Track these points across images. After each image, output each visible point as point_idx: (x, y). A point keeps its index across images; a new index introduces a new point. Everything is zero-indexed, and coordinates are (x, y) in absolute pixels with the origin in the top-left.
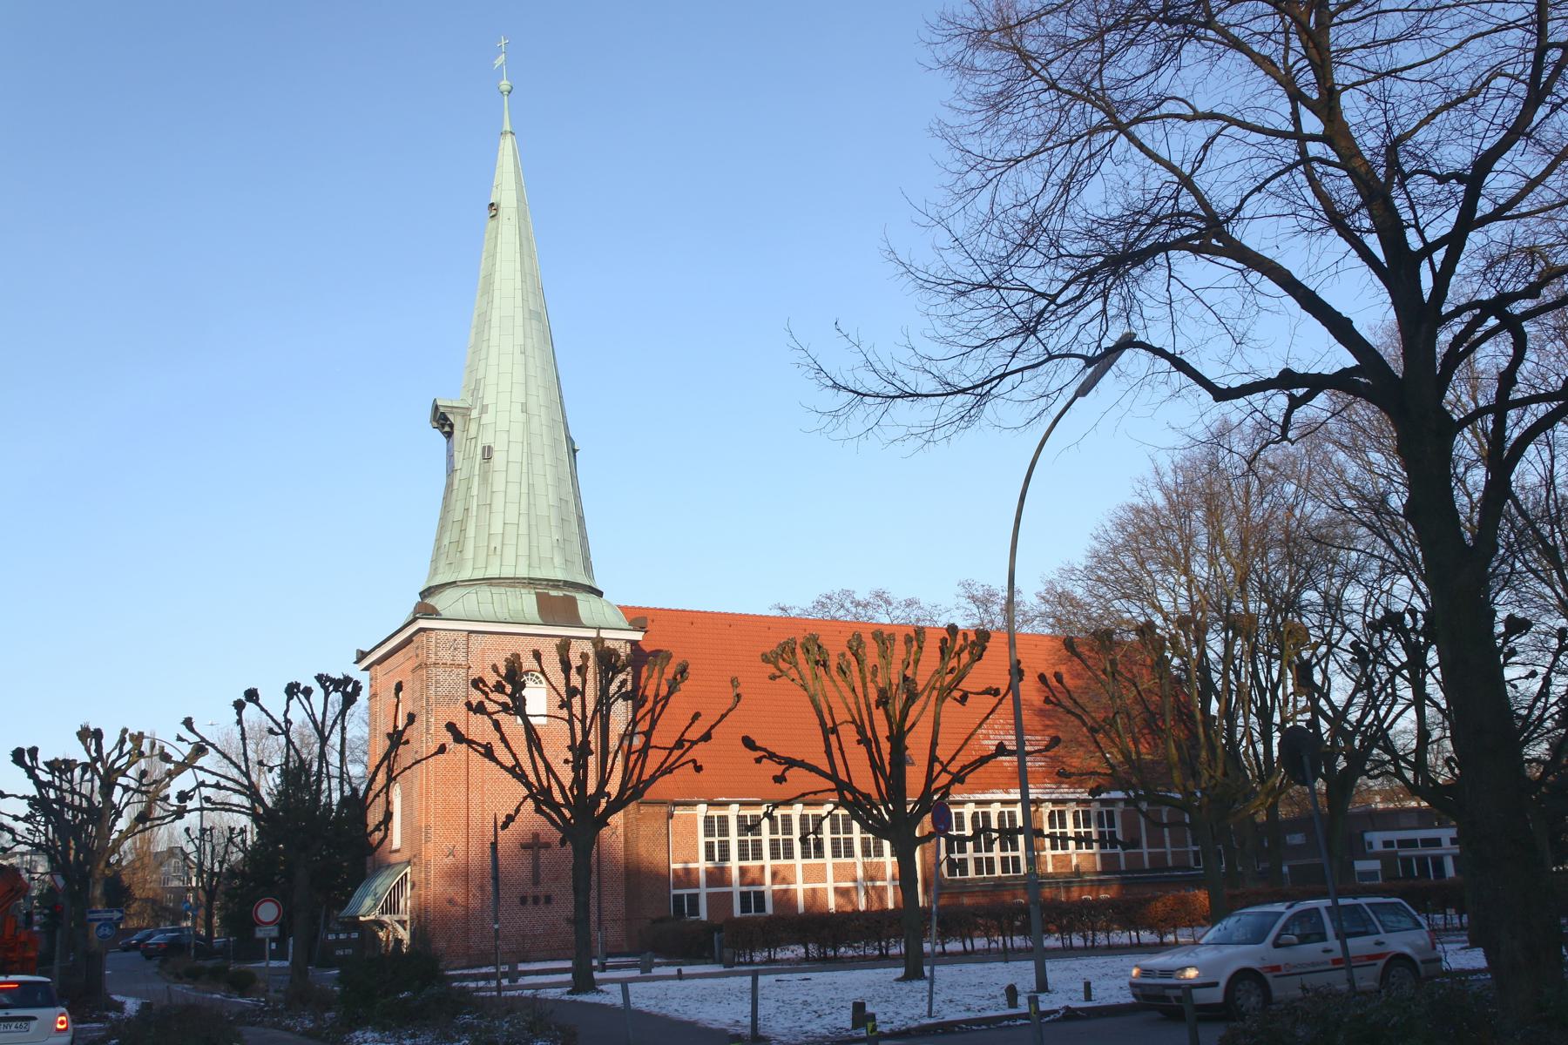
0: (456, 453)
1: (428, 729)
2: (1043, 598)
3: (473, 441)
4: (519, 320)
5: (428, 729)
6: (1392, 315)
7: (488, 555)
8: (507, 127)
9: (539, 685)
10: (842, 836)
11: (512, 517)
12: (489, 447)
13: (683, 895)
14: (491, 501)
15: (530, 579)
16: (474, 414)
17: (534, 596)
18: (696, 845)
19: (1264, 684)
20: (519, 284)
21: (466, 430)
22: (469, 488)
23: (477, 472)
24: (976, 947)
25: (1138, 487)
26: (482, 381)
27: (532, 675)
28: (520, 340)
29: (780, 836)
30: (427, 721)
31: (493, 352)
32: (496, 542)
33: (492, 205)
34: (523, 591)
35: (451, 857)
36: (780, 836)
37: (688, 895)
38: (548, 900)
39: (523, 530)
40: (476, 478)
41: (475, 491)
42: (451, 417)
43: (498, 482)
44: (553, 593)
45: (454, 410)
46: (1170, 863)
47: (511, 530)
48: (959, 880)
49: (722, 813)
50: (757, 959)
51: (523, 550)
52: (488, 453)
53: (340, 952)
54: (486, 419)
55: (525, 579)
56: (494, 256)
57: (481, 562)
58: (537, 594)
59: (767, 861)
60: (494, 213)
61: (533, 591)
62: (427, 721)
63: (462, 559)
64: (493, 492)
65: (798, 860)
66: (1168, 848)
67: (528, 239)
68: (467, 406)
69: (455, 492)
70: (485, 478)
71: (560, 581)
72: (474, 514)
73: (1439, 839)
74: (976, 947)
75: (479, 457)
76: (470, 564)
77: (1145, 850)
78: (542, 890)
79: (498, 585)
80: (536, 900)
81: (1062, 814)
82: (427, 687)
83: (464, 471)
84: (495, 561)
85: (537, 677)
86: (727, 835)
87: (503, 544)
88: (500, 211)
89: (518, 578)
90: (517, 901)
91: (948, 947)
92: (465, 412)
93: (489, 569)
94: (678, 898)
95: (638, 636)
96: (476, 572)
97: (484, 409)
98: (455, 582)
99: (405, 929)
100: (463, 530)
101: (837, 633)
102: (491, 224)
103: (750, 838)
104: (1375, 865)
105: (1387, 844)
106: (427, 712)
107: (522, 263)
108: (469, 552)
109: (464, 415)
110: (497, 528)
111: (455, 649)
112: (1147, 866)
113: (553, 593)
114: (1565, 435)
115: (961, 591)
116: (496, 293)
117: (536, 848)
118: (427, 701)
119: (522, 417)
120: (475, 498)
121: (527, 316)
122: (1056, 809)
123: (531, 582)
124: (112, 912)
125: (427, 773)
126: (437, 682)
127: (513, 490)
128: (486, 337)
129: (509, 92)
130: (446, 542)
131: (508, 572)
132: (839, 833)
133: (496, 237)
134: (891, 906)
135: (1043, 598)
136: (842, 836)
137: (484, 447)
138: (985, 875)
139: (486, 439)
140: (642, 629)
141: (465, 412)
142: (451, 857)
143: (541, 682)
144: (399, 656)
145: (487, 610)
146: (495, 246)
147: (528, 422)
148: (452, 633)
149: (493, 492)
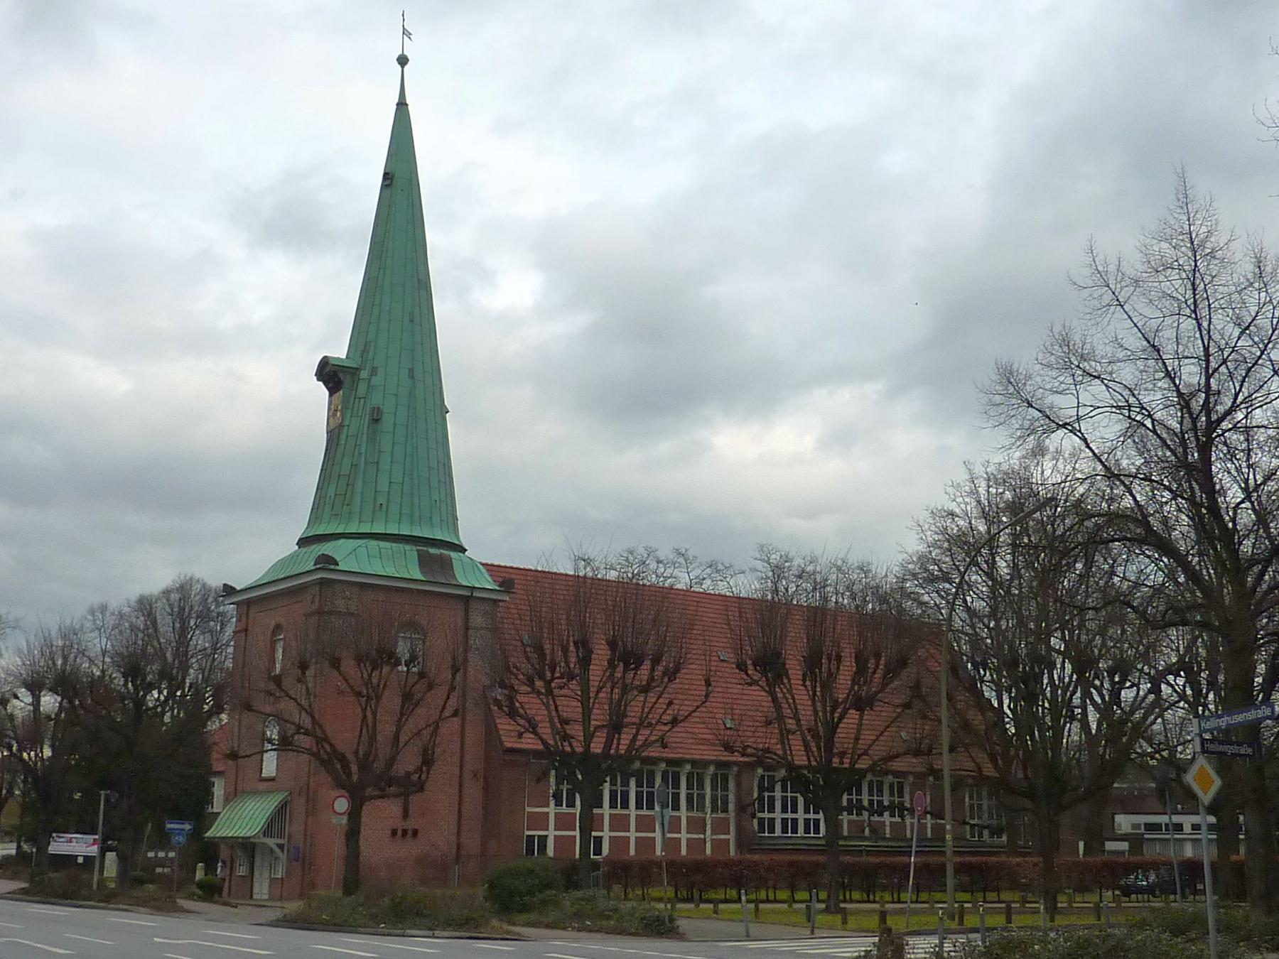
3: (362, 400)
7: (374, 511)
12: (378, 408)
13: (534, 836)
14: (378, 459)
16: (364, 374)
17: (416, 553)
19: (1057, 682)
23: (365, 431)
25: (951, 490)
26: (373, 344)
29: (975, 802)
37: (539, 836)
38: (415, 832)
40: (365, 436)
42: (341, 376)
43: (386, 445)
46: (929, 835)
53: (159, 870)
54: (376, 380)
58: (418, 550)
59: (633, 811)
61: (414, 548)
68: (355, 366)
70: (373, 437)
72: (362, 470)
73: (1181, 825)
78: (410, 824)
80: (405, 833)
81: (881, 783)
90: (420, 835)
94: (531, 838)
97: (374, 372)
99: (283, 851)
104: (1124, 846)
105: (1135, 826)
110: (384, 485)
112: (929, 835)
122: (766, 774)
124: (184, 824)
132: (787, 792)
134: (1215, 837)
138: (767, 835)
139: (376, 400)
149: (380, 452)
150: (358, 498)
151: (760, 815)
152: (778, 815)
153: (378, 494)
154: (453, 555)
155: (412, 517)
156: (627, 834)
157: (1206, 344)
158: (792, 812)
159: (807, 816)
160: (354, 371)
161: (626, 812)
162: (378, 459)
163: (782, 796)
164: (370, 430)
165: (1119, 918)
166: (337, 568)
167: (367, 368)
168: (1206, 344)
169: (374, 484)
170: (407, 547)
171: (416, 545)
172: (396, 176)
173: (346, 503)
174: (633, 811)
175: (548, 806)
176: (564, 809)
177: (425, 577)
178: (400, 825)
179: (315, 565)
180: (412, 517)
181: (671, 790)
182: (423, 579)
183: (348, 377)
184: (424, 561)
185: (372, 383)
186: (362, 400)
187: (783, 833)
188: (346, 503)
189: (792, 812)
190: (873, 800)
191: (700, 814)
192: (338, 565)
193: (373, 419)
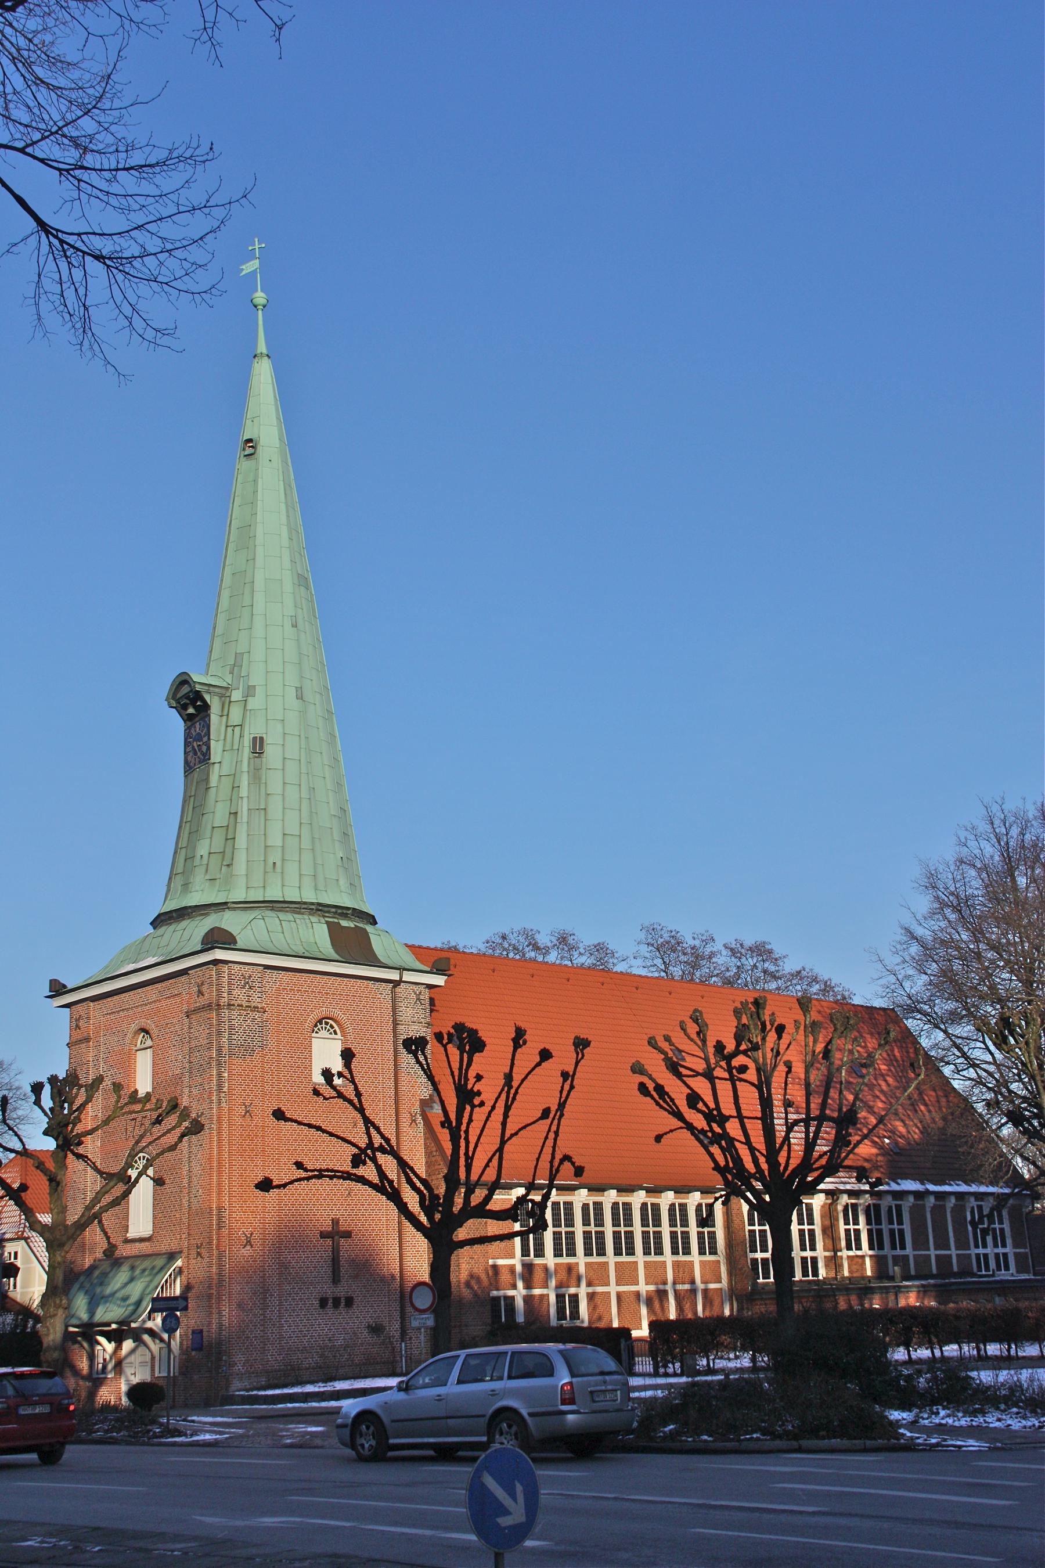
0: (212, 743)
1: (220, 1086)
2: (732, 950)
3: (237, 730)
4: (288, 586)
5: (220, 1086)
7: (265, 872)
8: (262, 347)
9: (333, 1036)
11: (293, 828)
12: (261, 739)
14: (266, 805)
15: (319, 904)
16: (236, 695)
20: (285, 542)
21: (225, 714)
22: (235, 788)
23: (245, 768)
24: (989, 1353)
25: (963, 834)
26: (246, 656)
27: (327, 1023)
28: (290, 611)
29: (593, 1228)
30: (220, 1075)
31: (259, 623)
32: (275, 857)
33: (250, 440)
34: (314, 919)
35: (248, 1247)
36: (593, 1228)
38: (349, 1302)
39: (306, 844)
41: (244, 792)
42: (207, 697)
44: (344, 923)
45: (211, 689)
46: (955, 1269)
48: (763, 1284)
49: (568, 1198)
50: (670, 1370)
51: (307, 870)
52: (258, 746)
54: (253, 703)
55: (312, 904)
56: (253, 503)
57: (257, 879)
58: (327, 923)
59: (611, 1258)
60: (251, 451)
62: (220, 1075)
63: (232, 876)
64: (285, 758)
65: (611, 1258)
66: (909, 1251)
67: (290, 486)
68: (225, 685)
69: (213, 791)
71: (348, 908)
72: (245, 819)
74: (989, 1353)
75: (247, 752)
76: (242, 882)
77: (953, 1252)
78: (341, 1291)
79: (281, 910)
80: (336, 1302)
82: (219, 1033)
83: (225, 764)
84: (275, 880)
85: (332, 1026)
86: (660, 1225)
87: (283, 860)
88: (259, 449)
89: (305, 903)
90: (316, 1303)
91: (914, 1355)
92: (224, 693)
93: (268, 889)
95: (439, 980)
96: (252, 892)
97: (250, 691)
98: (226, 903)
100: (230, 839)
101: (565, 981)
102: (245, 465)
103: (706, 1230)
106: (219, 1064)
107: (288, 516)
108: (240, 866)
109: (221, 696)
111: (250, 987)
113: (344, 923)
115: (642, 936)
116: (260, 551)
118: (219, 1050)
119: (296, 704)
120: (245, 800)
121: (296, 581)
123: (320, 909)
125: (219, 1141)
126: (231, 1028)
127: (292, 792)
128: (247, 602)
129: (264, 306)
130: (203, 849)
131: (292, 895)
133: (255, 481)
135: (732, 950)
137: (255, 739)
139: (255, 728)
140: (440, 971)
141: (224, 693)
142: (248, 1247)
143: (335, 1033)
144: (152, 992)
145: (280, 942)
146: (255, 492)
147: (303, 713)
148: (247, 967)
151: (752, 1255)
152: (611, 1258)
154: (369, 928)
155: (315, 879)
159: (996, 1251)
160: (223, 691)
161: (659, 1258)
162: (266, 805)
163: (902, 1224)
164: (252, 767)
165: (965, 1348)
167: (241, 688)
169: (263, 837)
171: (324, 917)
172: (262, 443)
174: (611, 1258)
175: (937, 1256)
180: (315, 879)
185: (249, 707)
187: (803, 1276)
188: (225, 863)
190: (850, 1230)
191: (712, 1258)
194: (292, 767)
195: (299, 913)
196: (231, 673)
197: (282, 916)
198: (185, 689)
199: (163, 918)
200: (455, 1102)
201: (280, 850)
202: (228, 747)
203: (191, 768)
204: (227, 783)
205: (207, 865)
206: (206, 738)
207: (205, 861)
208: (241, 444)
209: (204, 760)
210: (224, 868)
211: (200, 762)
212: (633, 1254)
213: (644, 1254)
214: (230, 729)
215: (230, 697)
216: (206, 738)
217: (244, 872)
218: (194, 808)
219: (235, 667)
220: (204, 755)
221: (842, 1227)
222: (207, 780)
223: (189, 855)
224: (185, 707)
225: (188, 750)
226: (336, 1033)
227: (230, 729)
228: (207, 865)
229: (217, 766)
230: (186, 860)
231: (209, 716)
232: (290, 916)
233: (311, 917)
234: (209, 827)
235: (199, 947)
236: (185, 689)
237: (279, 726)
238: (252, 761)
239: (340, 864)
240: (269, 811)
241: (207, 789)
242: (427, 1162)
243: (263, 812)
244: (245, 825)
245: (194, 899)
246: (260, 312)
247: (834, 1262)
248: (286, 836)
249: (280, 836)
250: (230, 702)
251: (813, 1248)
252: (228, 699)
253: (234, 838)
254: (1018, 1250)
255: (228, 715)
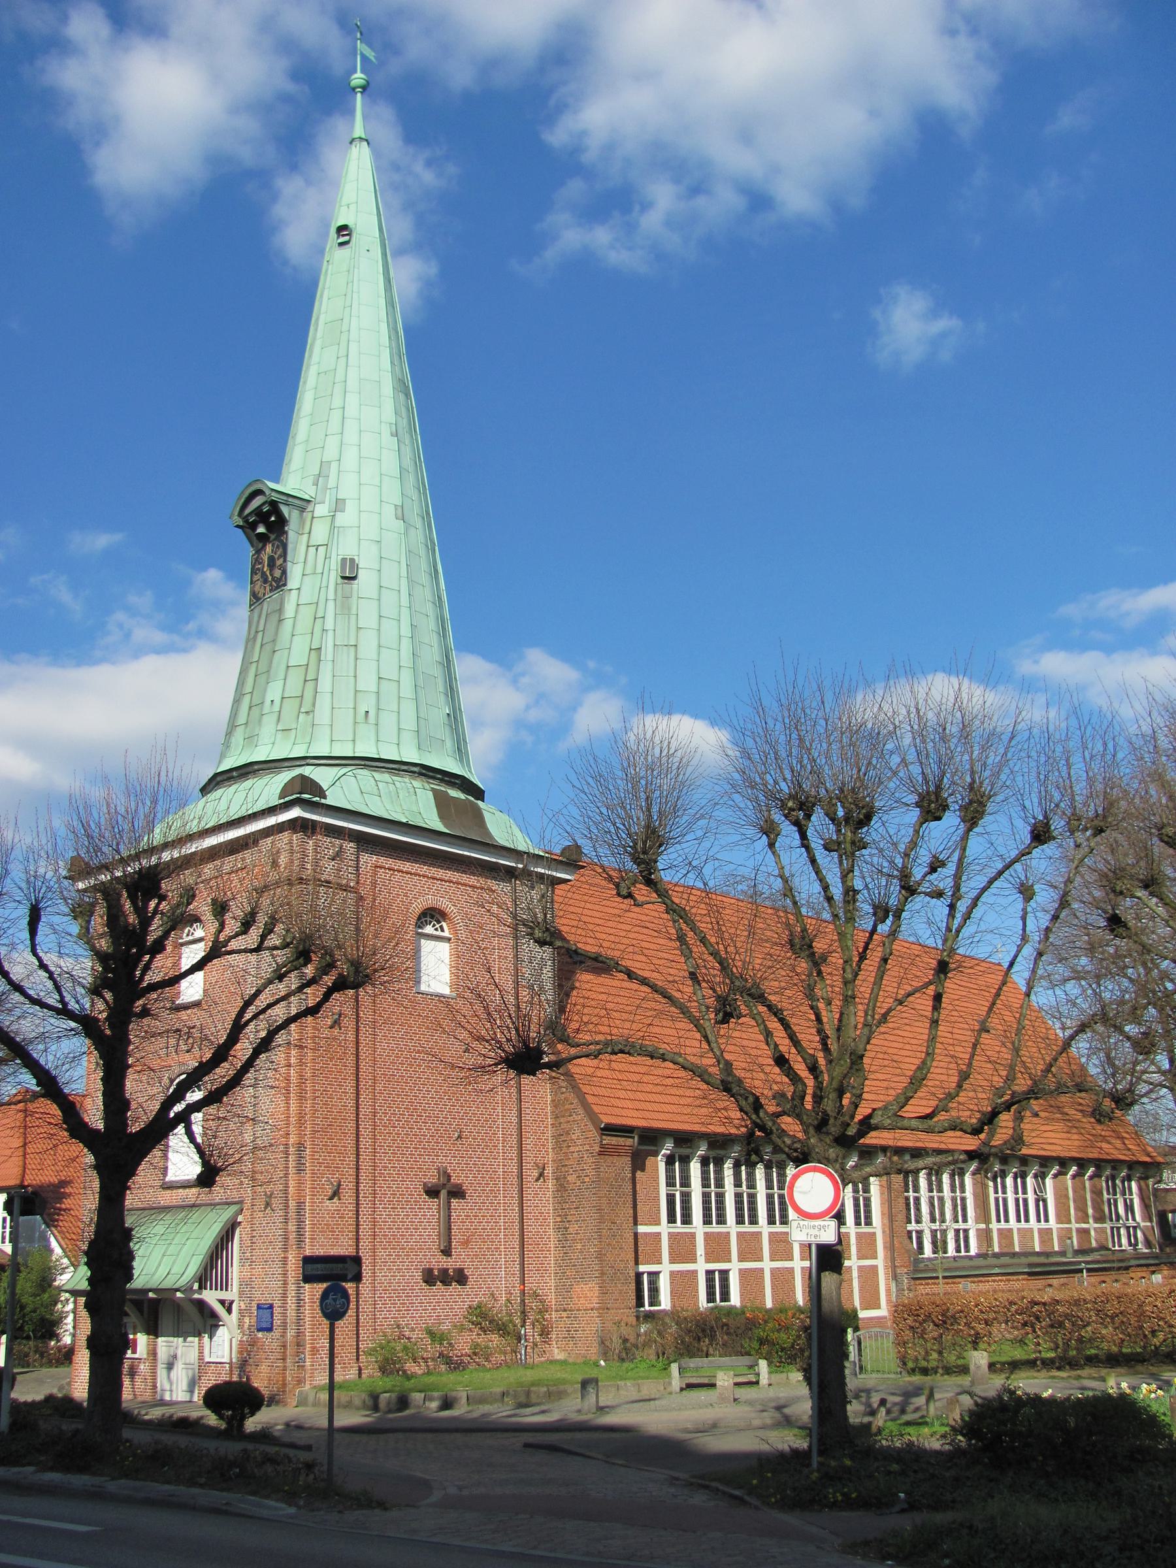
3: (322, 550)
6: (87, 1119)
8: (359, 131)
10: (1074, 1226)
11: (389, 672)
12: (352, 560)
16: (321, 510)
18: (657, 1198)
23: (331, 595)
26: (334, 466)
29: (1020, 1195)
39: (407, 690)
40: (331, 604)
42: (285, 510)
43: (367, 615)
47: (388, 688)
51: (409, 723)
58: (433, 790)
60: (346, 238)
64: (358, 628)
69: (287, 625)
70: (345, 605)
72: (330, 657)
75: (334, 577)
78: (450, 1264)
88: (354, 235)
97: (339, 505)
100: (311, 680)
108: (323, 713)
114: (2, 1134)
117: (443, 1194)
120: (331, 633)
123: (427, 772)
130: (274, 692)
136: (1074, 1226)
137: (344, 560)
139: (346, 547)
150: (324, 703)
153: (358, 694)
156: (787, 1264)
157: (248, 1016)
158: (718, 1223)
166: (323, 801)
168: (248, 1016)
169: (352, 679)
170: (417, 783)
173: (303, 710)
176: (679, 1227)
177: (446, 826)
178: (439, 1262)
179: (280, 799)
181: (1020, 1195)
182: (440, 827)
183: (295, 513)
184: (442, 803)
186: (308, 570)
188: (303, 710)
189: (718, 1223)
192: (325, 798)
193: (344, 578)
194: (389, 598)
195: (398, 775)
196: (316, 484)
197: (376, 775)
198: (257, 502)
199: (219, 779)
200: (96, 1184)
201: (373, 698)
202: (308, 570)
203: (258, 599)
204: (306, 613)
205: (280, 712)
206: (281, 560)
207: (276, 708)
208: (333, 230)
209: (278, 587)
210: (302, 716)
211: (271, 591)
212: (725, 1223)
213: (704, 1224)
214: (312, 550)
215: (313, 512)
216: (281, 560)
217: (327, 721)
218: (262, 645)
219: (320, 478)
220: (278, 581)
221: (992, 1196)
222: (280, 610)
223: (256, 701)
224: (253, 526)
225: (254, 579)
226: (443, 930)
227: (312, 550)
228: (280, 712)
229: (294, 593)
230: (250, 708)
231: (286, 533)
232: (386, 777)
233: (413, 782)
234: (284, 667)
235: (275, 801)
236: (257, 502)
237: (374, 548)
238: (340, 587)
239: (446, 722)
240: (360, 648)
241: (280, 621)
242: (553, 1101)
243: (352, 649)
244: (330, 663)
245: (260, 755)
246: (359, 95)
247: (985, 1236)
248: (381, 680)
249: (375, 678)
250: (313, 517)
251: (965, 1220)
252: (310, 514)
253: (316, 679)
254: (1061, 1226)
255: (310, 533)
